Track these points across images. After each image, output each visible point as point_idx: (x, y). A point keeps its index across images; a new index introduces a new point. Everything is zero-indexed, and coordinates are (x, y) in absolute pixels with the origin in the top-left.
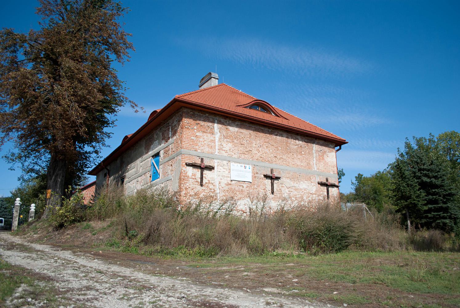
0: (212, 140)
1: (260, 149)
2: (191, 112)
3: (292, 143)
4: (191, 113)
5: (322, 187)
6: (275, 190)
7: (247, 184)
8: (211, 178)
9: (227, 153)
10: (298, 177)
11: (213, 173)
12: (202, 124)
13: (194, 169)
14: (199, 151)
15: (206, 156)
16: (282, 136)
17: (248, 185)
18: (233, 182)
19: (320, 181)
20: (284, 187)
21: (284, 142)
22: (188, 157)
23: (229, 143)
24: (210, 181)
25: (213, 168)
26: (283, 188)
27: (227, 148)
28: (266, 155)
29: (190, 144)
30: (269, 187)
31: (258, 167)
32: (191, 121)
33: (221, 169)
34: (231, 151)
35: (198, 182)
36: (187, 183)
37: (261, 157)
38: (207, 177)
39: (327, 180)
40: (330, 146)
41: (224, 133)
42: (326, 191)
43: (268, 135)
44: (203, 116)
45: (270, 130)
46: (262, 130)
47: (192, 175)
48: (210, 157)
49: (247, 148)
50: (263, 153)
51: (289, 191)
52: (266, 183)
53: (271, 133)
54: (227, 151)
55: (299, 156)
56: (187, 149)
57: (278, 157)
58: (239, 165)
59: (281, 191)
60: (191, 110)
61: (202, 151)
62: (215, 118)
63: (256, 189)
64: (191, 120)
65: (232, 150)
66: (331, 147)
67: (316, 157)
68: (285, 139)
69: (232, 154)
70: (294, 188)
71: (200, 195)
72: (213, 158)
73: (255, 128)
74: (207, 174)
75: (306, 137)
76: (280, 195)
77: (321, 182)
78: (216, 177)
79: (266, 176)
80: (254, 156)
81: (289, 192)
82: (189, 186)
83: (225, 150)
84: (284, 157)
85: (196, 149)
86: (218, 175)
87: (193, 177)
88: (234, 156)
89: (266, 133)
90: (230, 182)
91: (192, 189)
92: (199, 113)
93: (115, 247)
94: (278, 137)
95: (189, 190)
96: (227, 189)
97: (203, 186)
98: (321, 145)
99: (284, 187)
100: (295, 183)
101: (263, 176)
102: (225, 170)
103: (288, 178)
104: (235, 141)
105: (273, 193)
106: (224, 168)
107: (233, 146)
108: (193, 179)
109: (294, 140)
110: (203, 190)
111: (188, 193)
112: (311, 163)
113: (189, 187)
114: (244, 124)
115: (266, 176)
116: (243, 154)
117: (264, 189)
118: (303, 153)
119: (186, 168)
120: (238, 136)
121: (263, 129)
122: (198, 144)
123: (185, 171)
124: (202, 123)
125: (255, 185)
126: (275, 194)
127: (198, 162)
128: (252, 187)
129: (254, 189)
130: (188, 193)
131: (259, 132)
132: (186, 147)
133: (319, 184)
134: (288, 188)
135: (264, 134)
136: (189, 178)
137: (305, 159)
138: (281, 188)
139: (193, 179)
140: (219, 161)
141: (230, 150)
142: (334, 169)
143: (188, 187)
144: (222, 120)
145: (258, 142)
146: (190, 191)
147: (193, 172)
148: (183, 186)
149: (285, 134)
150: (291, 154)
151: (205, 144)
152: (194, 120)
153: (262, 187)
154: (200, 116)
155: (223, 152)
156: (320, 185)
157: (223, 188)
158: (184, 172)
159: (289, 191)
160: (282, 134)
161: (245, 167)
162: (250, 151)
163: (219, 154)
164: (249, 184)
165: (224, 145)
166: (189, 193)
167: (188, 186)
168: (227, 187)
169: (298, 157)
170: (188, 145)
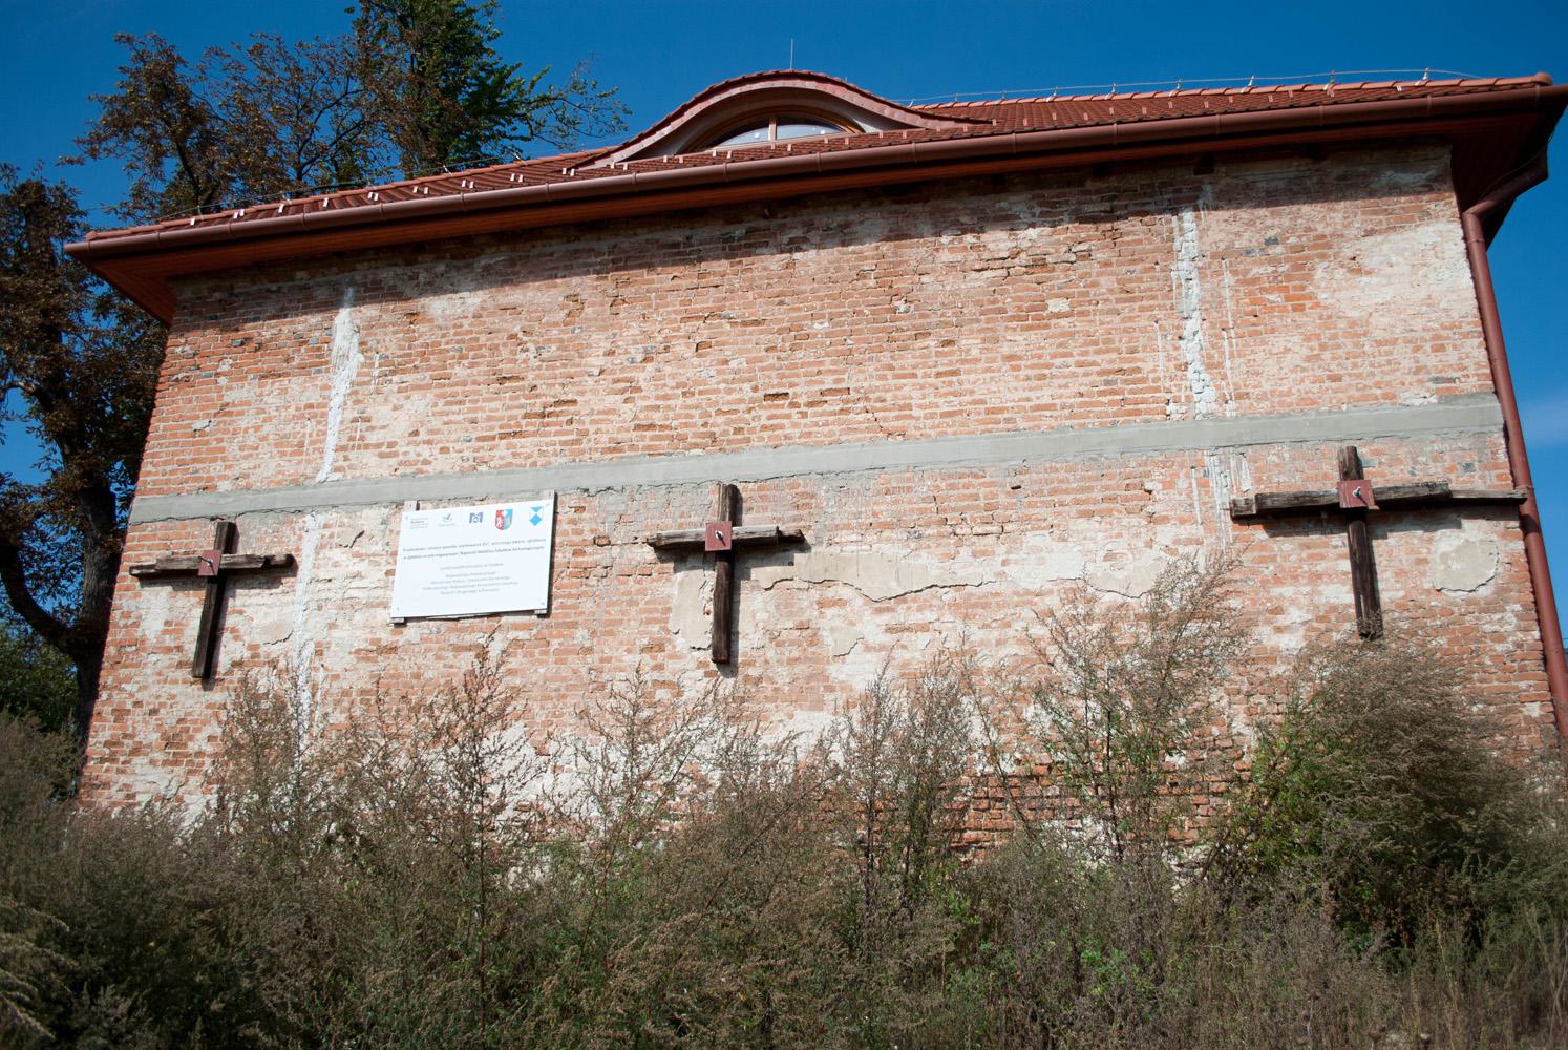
0: (310, 406)
1: (642, 376)
2: (213, 290)
3: (945, 256)
4: (217, 295)
5: (1289, 547)
6: (744, 645)
7: (516, 627)
8: (265, 630)
9: (395, 454)
10: (1003, 499)
11: (289, 598)
12: (267, 334)
13: (180, 594)
14: (224, 486)
15: (260, 507)
16: (844, 236)
17: (522, 635)
18: (412, 632)
19: (1248, 487)
20: (839, 602)
21: (862, 275)
22: (160, 533)
23: (416, 395)
24: (263, 650)
25: (289, 565)
26: (830, 612)
27: (399, 427)
28: (690, 401)
29: (182, 463)
30: (695, 628)
31: (612, 497)
32: (208, 339)
33: (336, 565)
34: (423, 436)
35: (735, 519)
36: (128, 680)
37: (651, 427)
38: (243, 630)
39: (1352, 468)
40: (1389, 175)
41: (390, 343)
42: (1346, 565)
43: (723, 265)
44: (279, 290)
45: (739, 231)
46: (676, 245)
47: (165, 632)
48: (279, 505)
49: (542, 389)
50: (666, 397)
51: (889, 630)
52: (674, 603)
53: (733, 250)
54: (391, 445)
55: (1018, 341)
56: (160, 492)
57: (802, 391)
58: (464, 511)
59: (814, 640)
60: (210, 284)
61: (242, 483)
62: (346, 277)
63: (590, 650)
64: (210, 333)
65: (432, 432)
66: (1396, 190)
67: (1212, 304)
68: (869, 252)
69: (425, 451)
70: (951, 595)
71: (191, 738)
72: (335, 503)
73: (613, 249)
74: (249, 611)
75: (1089, 185)
76: (801, 669)
77: (1259, 498)
78: (300, 619)
79: (678, 552)
80: (585, 433)
81: (889, 639)
82: (139, 696)
83: (378, 446)
84: (854, 380)
85: (211, 479)
86: (313, 605)
87: (169, 641)
88: (441, 463)
89: (701, 260)
90: (386, 637)
91: (154, 712)
92: (253, 282)
93: (10, 913)
94: (812, 253)
95: (136, 719)
96: (361, 684)
97: (217, 688)
98: (1271, 199)
99: (839, 602)
100: (965, 552)
101: (649, 553)
102: (362, 567)
103: (889, 526)
104: (459, 372)
105: (725, 655)
106: (357, 555)
107: (441, 406)
108: (169, 650)
109: (969, 238)
110: (209, 706)
111: (126, 736)
112: (1154, 364)
113: (138, 704)
114: (540, 248)
115: (678, 552)
116: (502, 436)
117: (655, 647)
118: (1057, 305)
119: (137, 595)
120: (483, 338)
121: (677, 236)
122: (222, 450)
123: (127, 615)
124: (265, 330)
125: (574, 625)
126: (753, 672)
127: (1325, 482)
128: (555, 644)
129: (561, 657)
130: (126, 736)
131: (641, 266)
132: (155, 482)
133: (1241, 518)
134: (880, 605)
135: (677, 271)
136: (144, 650)
137: (1074, 346)
138: (811, 614)
139: (169, 650)
140: (332, 516)
141: (416, 433)
142: (1451, 357)
143: (129, 706)
144: (387, 275)
145: (634, 329)
146: (139, 726)
147: (170, 609)
148: (110, 697)
149: (876, 220)
150: (931, 342)
151: (264, 438)
152: (224, 329)
153: (635, 630)
154: (261, 297)
155: (370, 457)
156: (1259, 534)
157: (336, 677)
158: (122, 622)
159: (889, 630)
160: (847, 225)
161: (502, 521)
162: (559, 403)
163: (338, 475)
164: (528, 627)
165: (380, 412)
166: (132, 736)
167: (132, 695)
168: (365, 669)
169: (1005, 349)
170: (169, 468)
